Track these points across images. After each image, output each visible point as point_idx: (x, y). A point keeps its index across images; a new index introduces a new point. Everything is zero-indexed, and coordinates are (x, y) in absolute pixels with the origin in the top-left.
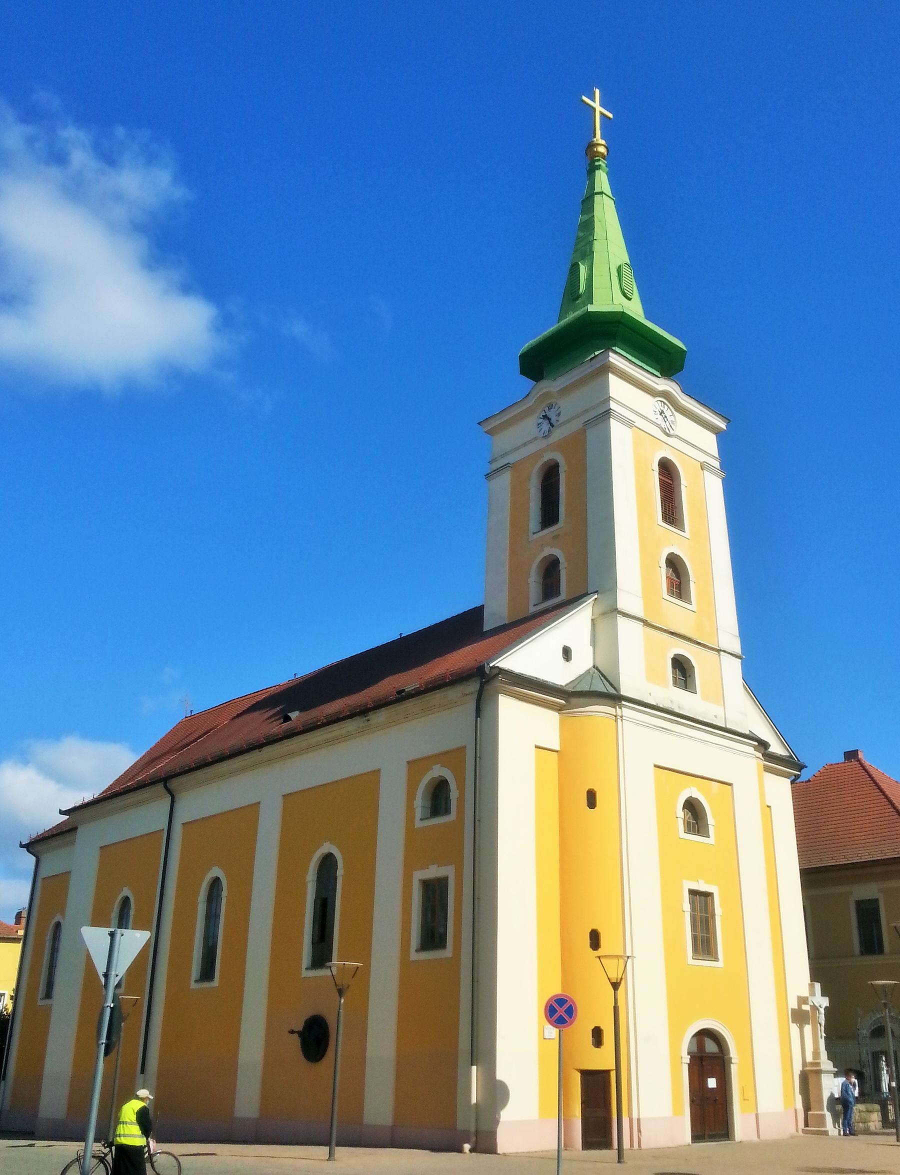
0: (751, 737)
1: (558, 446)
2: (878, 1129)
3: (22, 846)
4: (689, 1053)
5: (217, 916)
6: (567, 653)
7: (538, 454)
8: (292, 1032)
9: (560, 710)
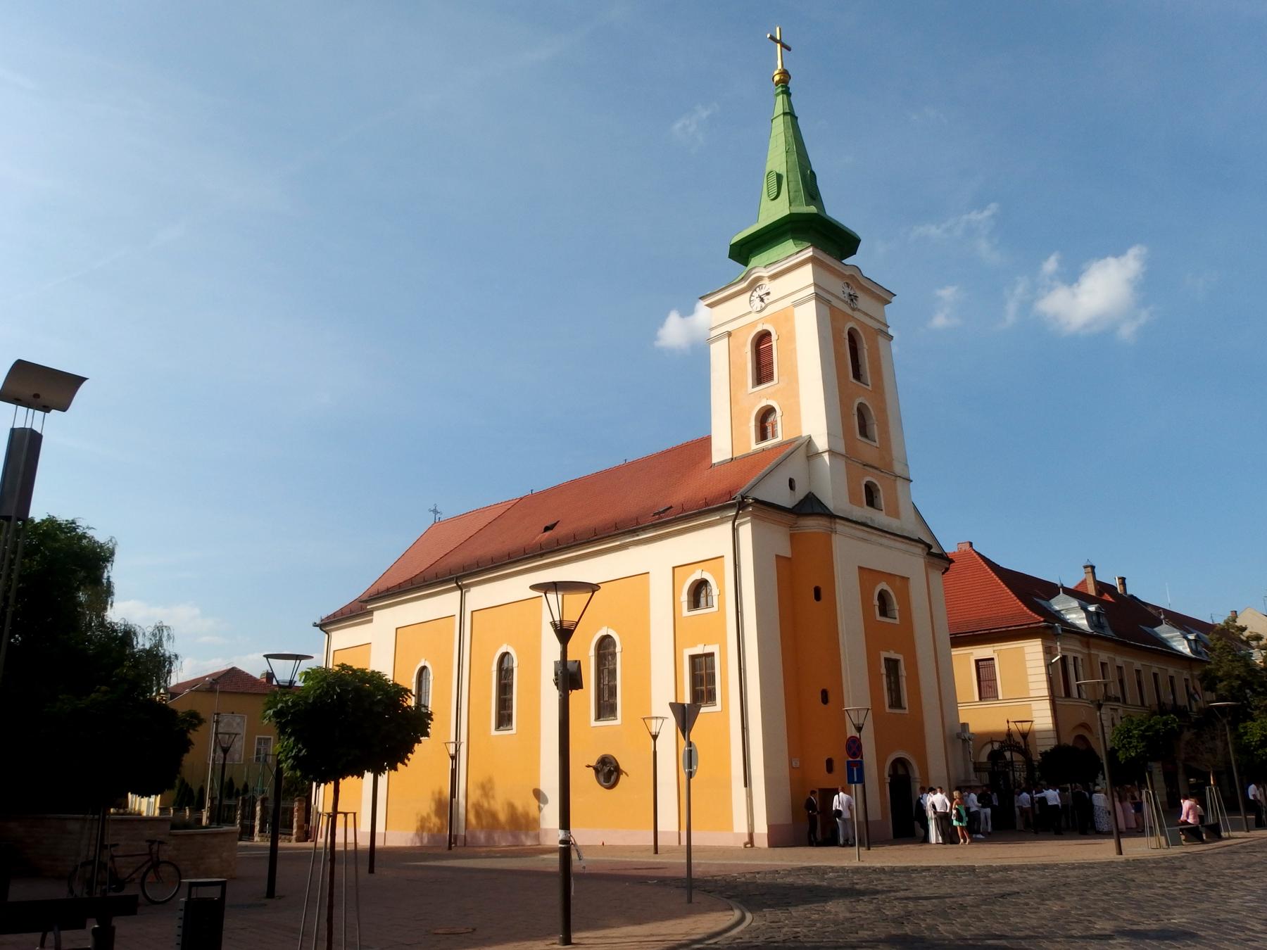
0: (920, 541)
1: (774, 318)
2: (768, 920)
3: (315, 625)
4: (889, 776)
5: (889, 689)
6: (791, 483)
7: (754, 324)
8: (588, 766)
9: (791, 527)
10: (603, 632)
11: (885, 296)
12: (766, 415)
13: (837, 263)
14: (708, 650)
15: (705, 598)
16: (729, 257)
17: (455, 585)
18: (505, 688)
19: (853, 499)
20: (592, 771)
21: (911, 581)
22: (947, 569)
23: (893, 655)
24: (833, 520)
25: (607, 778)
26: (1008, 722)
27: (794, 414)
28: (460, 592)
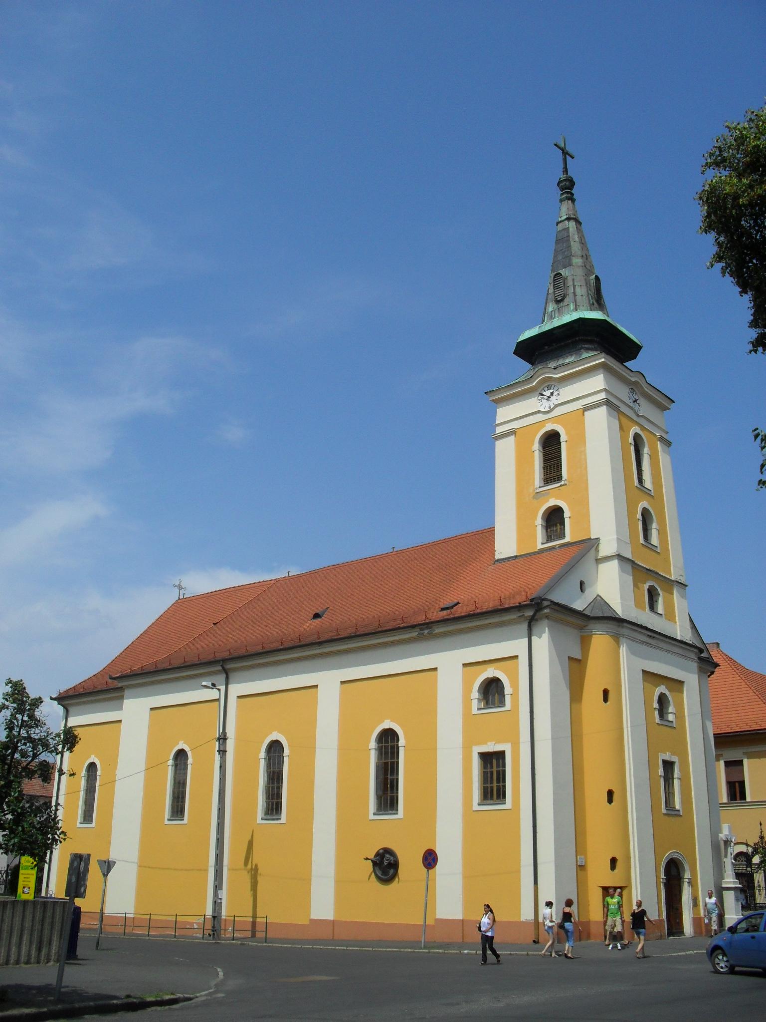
8: (367, 859)
10: (387, 724)
11: (665, 402)
12: (554, 518)
13: (618, 364)
14: (498, 748)
15: (626, 729)
16: (514, 353)
17: (221, 668)
18: (274, 778)
19: (638, 604)
20: (370, 863)
21: (685, 685)
22: (712, 673)
23: (667, 756)
24: (620, 624)
25: (385, 872)
26: (761, 824)
27: (584, 517)
28: (225, 676)
